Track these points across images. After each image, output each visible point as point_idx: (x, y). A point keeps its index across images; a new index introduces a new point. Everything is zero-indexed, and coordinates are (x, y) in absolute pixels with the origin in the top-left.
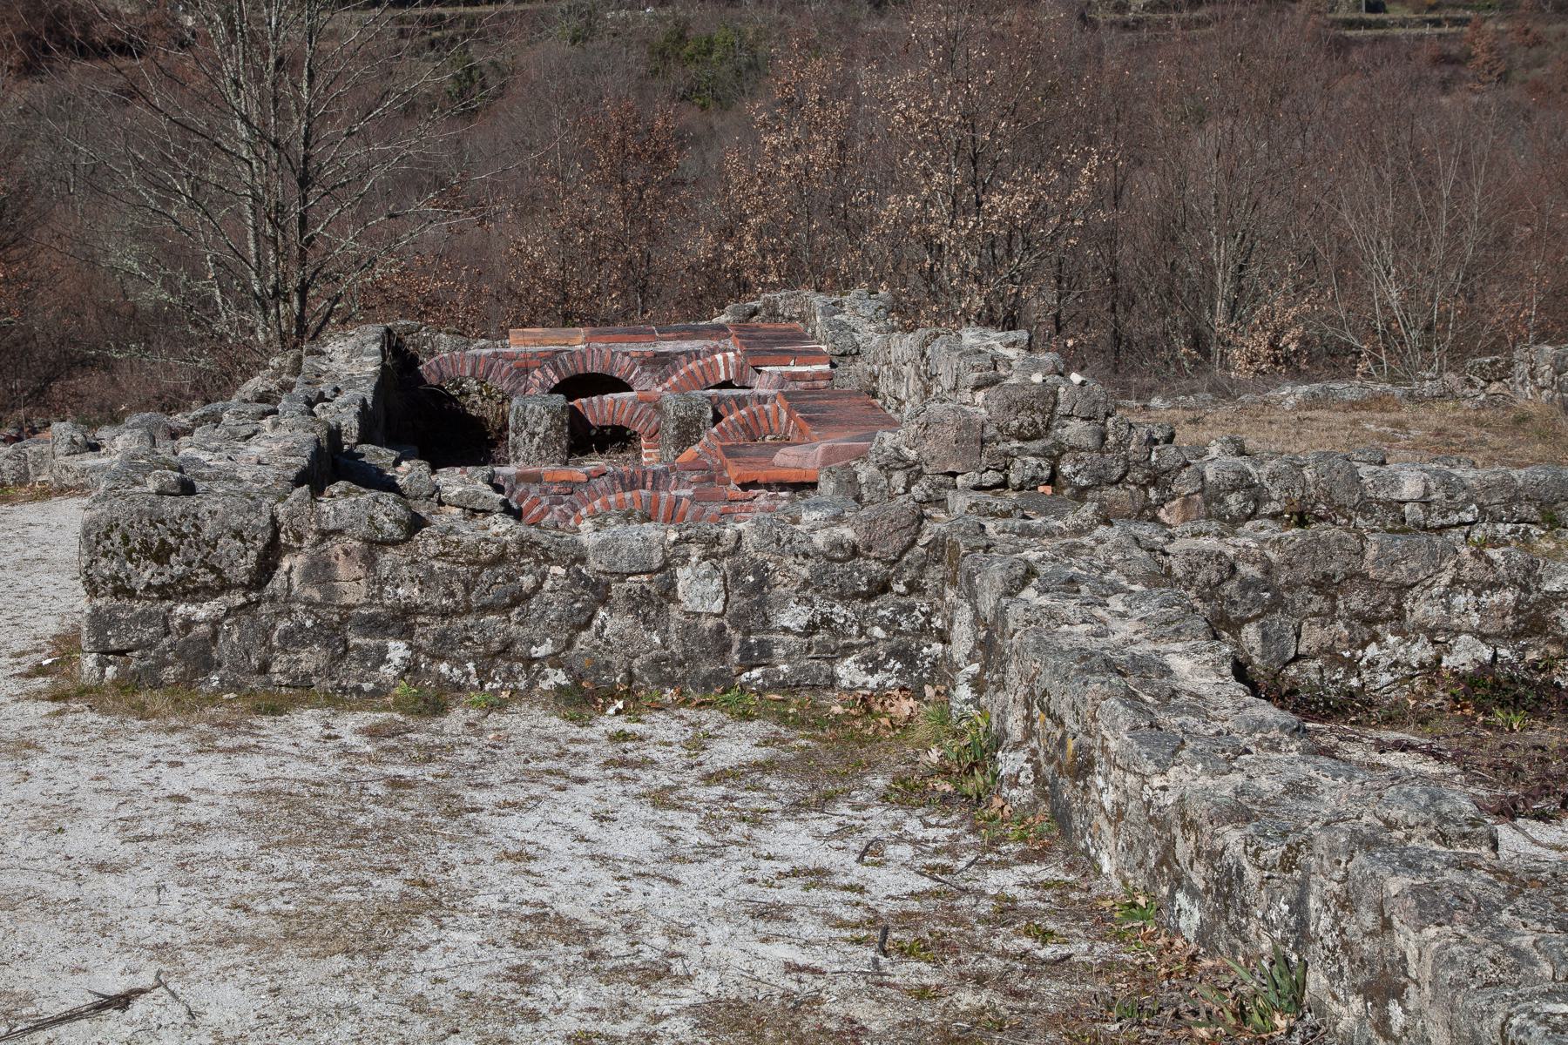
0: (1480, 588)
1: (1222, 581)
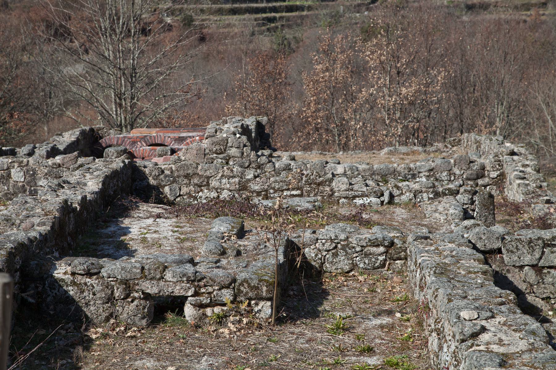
0: (229, 177)
1: (159, 175)
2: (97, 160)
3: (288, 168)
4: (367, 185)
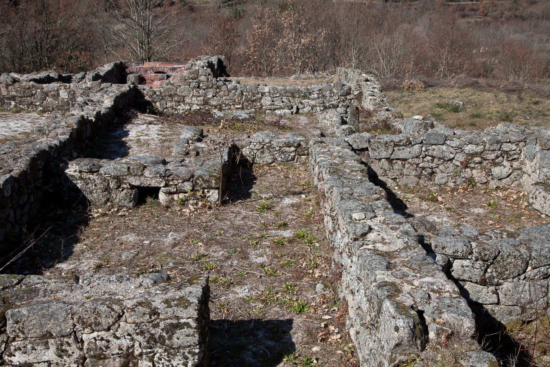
0: (197, 97)
2: (113, 85)
3: (235, 88)
4: (283, 102)
